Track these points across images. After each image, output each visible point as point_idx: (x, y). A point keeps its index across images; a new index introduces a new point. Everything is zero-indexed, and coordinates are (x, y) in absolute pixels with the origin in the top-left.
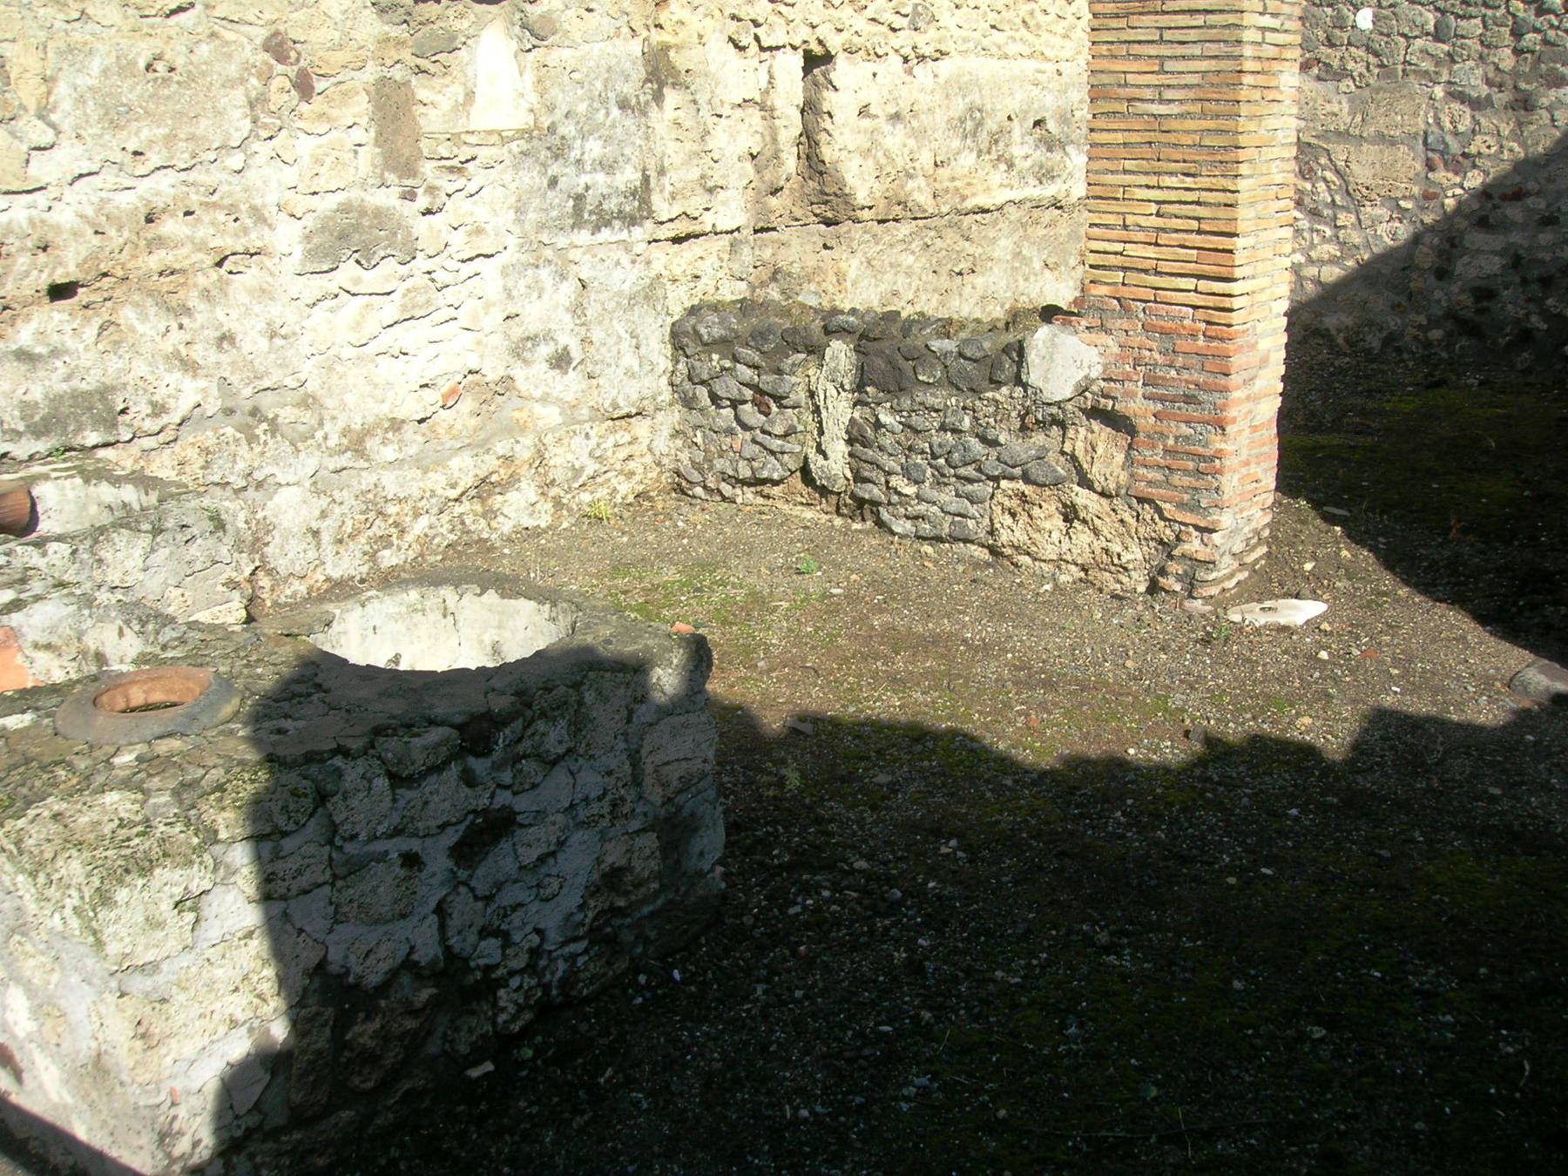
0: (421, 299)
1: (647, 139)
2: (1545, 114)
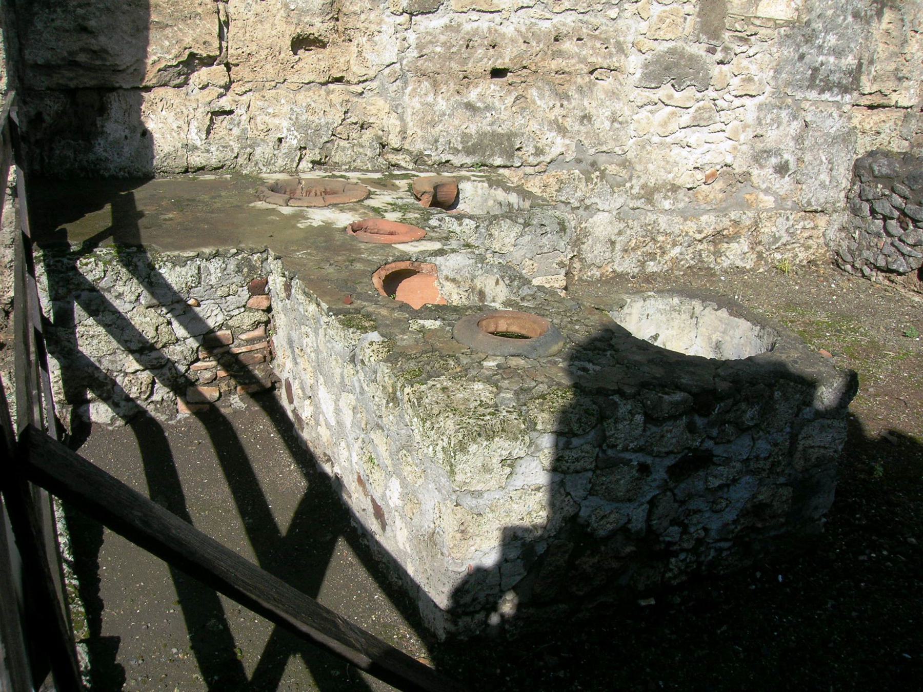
0: (706, 115)
1: (867, 39)
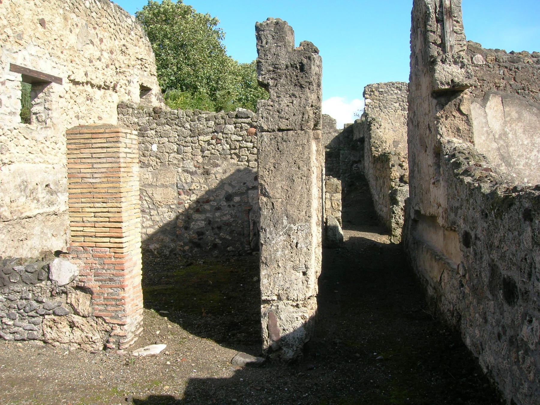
2: (213, 176)
